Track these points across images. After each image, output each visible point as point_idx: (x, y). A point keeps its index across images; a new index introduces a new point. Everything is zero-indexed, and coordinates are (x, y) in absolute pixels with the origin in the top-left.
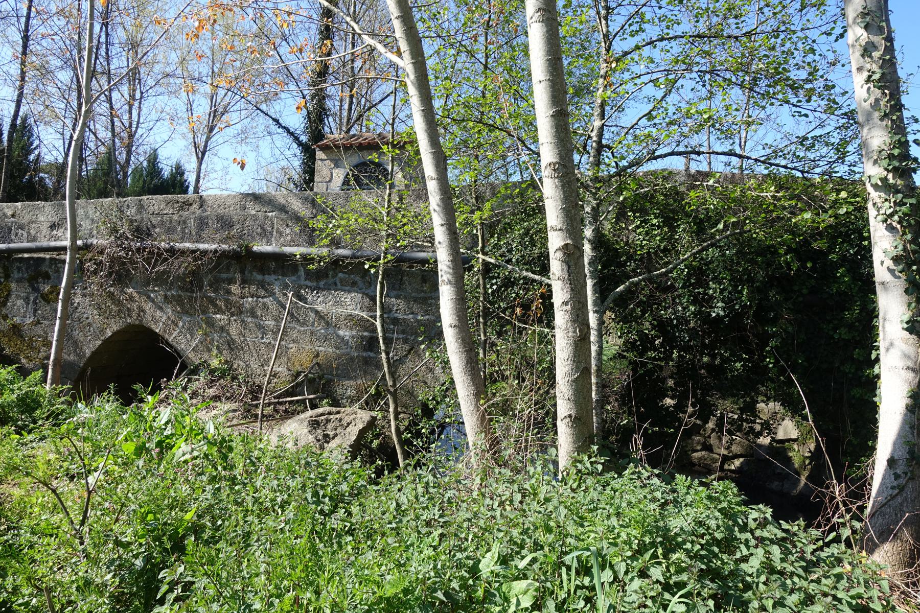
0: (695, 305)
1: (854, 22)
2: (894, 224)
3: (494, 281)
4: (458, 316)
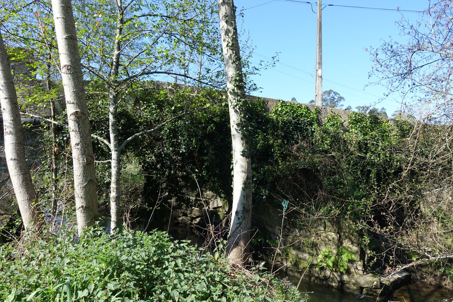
0: (172, 147)
1: (222, 19)
2: (237, 110)
3: (65, 135)
4: (17, 153)
